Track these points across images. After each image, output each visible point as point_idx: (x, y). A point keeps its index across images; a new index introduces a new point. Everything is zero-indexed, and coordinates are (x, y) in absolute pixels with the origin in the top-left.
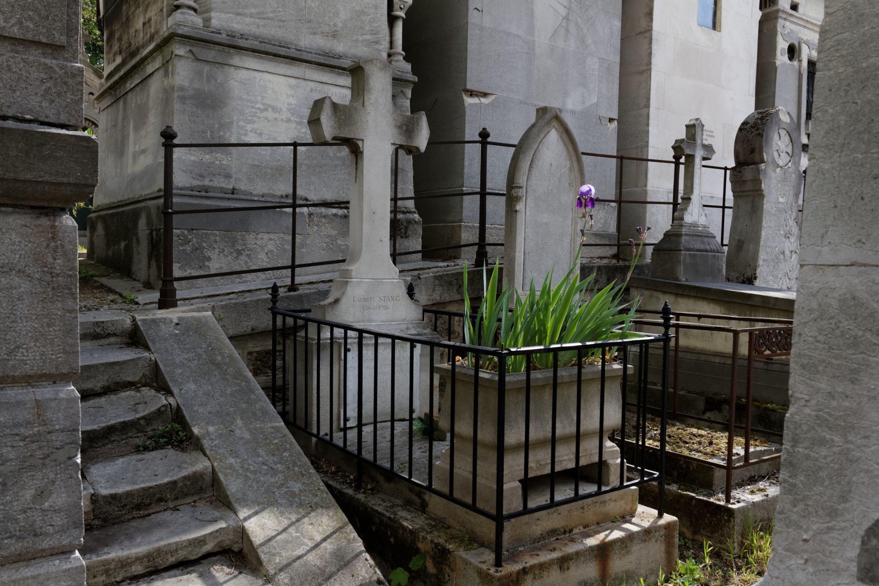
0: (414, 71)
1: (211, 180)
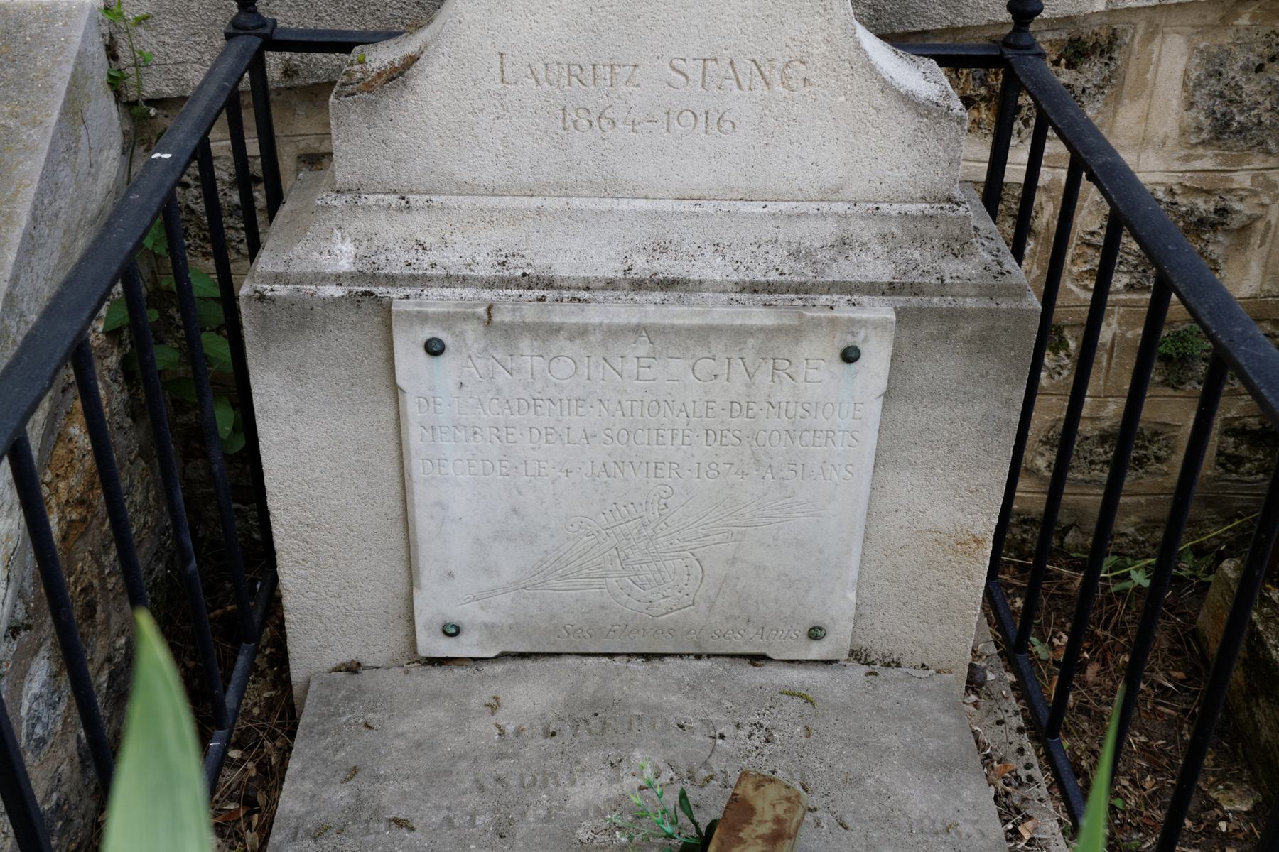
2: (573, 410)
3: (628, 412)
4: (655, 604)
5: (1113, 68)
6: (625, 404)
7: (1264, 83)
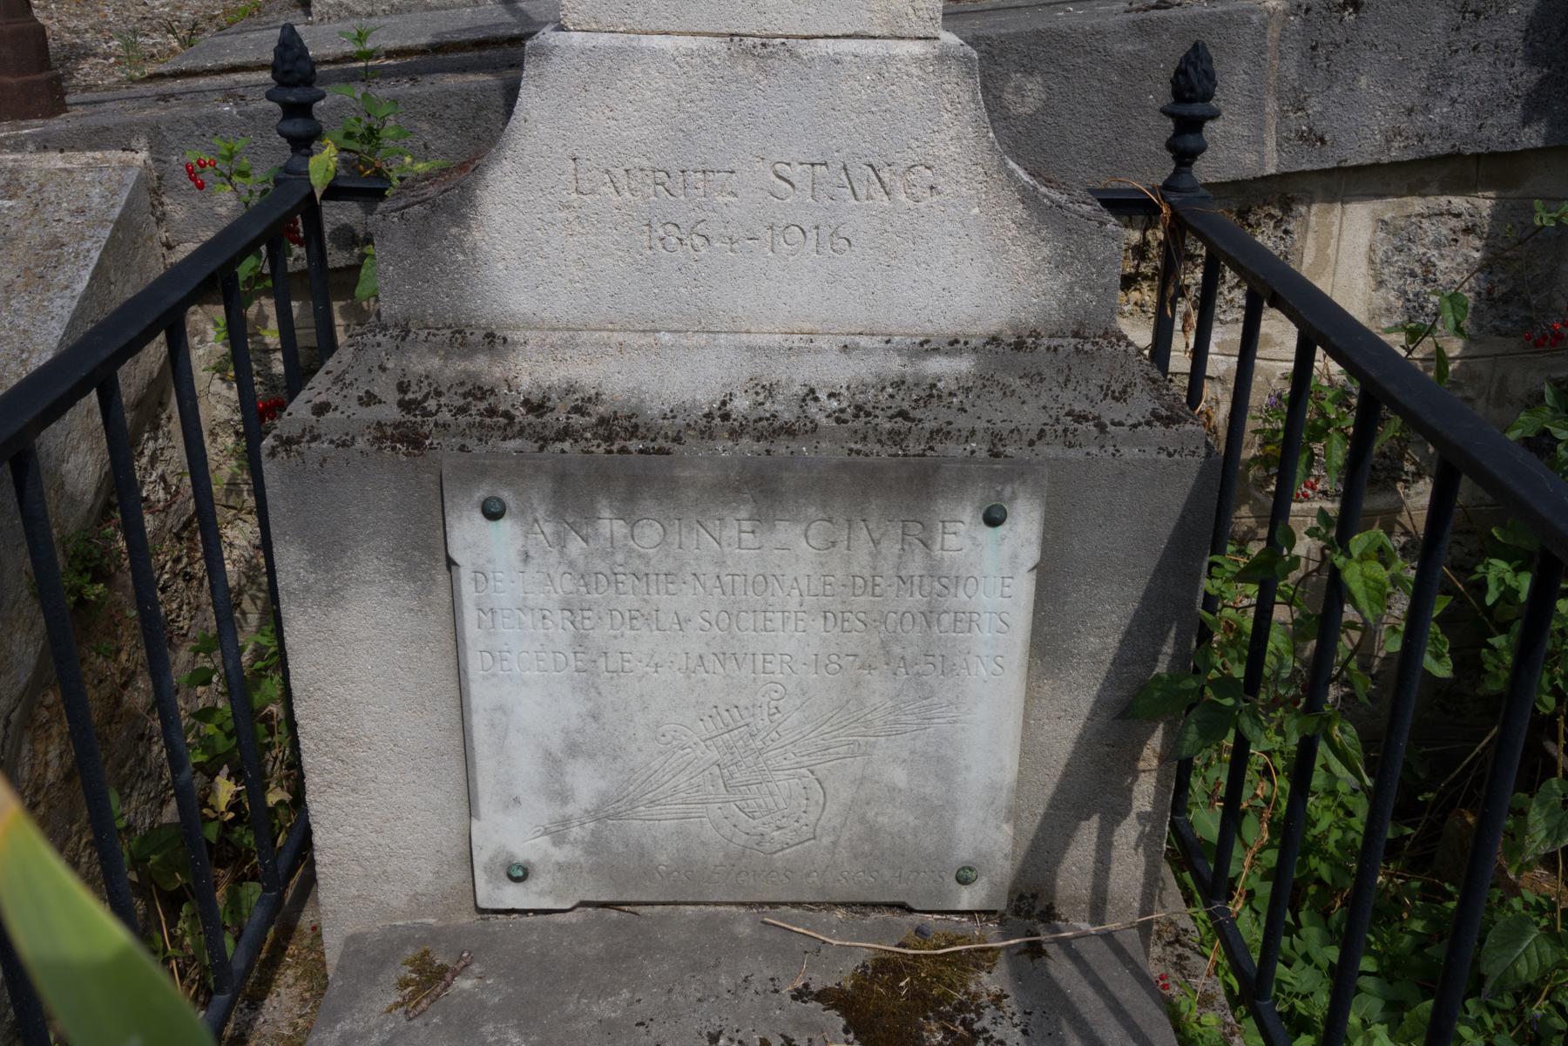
3: (729, 590)
4: (767, 838)
5: (1289, 242)
7: (1459, 259)
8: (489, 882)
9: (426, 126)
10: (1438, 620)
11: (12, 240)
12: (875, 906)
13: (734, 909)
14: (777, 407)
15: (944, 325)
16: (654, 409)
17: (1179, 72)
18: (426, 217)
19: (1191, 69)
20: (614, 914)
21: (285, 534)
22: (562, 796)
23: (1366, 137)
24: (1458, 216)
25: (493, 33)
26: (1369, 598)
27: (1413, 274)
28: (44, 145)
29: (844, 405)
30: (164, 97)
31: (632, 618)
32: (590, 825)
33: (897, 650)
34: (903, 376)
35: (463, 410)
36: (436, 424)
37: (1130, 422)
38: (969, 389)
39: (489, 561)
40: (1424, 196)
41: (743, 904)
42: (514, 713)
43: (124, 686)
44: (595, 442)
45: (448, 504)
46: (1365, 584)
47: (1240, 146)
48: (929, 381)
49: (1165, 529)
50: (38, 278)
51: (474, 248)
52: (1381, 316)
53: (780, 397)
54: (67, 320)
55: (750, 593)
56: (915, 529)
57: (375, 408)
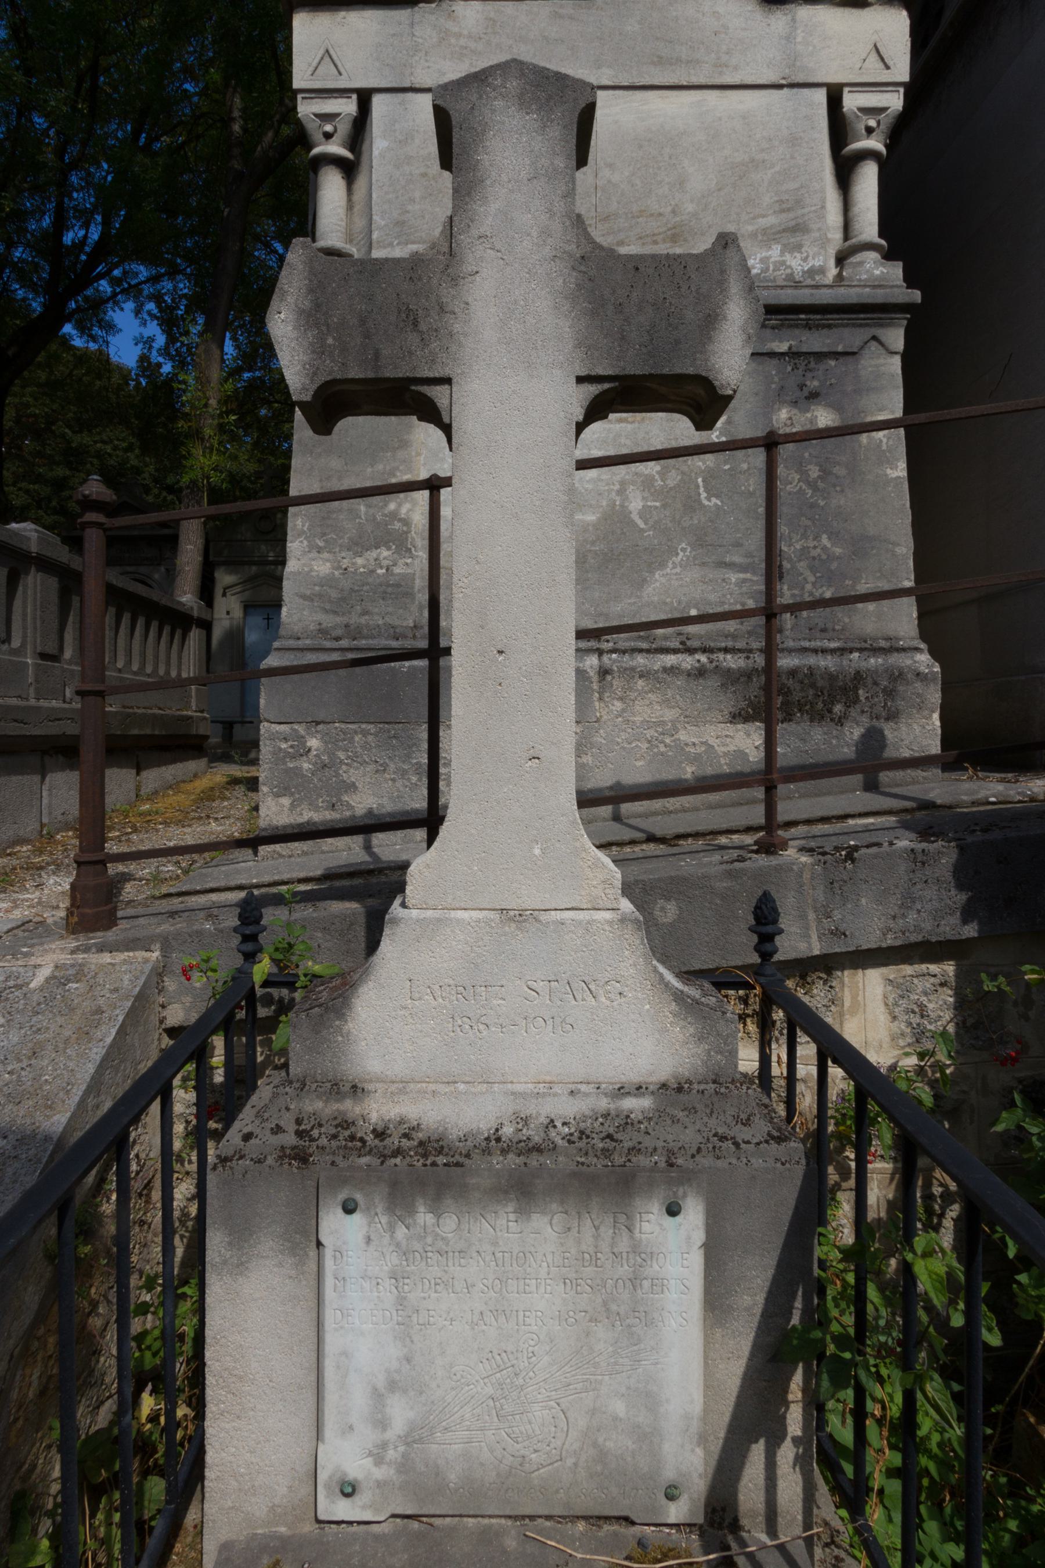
0: (911, 279)
1: (365, 613)
2: (456, 1260)
3: (500, 1263)
4: (527, 1459)
6: (499, 1255)
7: (941, 1003)
8: (327, 1497)
9: (320, 935)
10: (985, 1300)
11: (73, 1009)
12: (607, 1518)
13: (503, 1521)
14: (530, 1132)
15: (632, 1076)
16: (454, 1134)
17: (757, 908)
18: (322, 1015)
19: (764, 907)
20: (415, 1525)
21: (215, 1223)
22: (383, 1424)
23: (871, 932)
24: (935, 976)
25: (359, 868)
26: (934, 1288)
27: (913, 1012)
28: (101, 949)
29: (573, 1130)
30: (172, 914)
31: (436, 1284)
32: (401, 1449)
33: (614, 1307)
34: (609, 1110)
35: (334, 1137)
36: (318, 1147)
37: (755, 1141)
38: (650, 1119)
39: (344, 1243)
40: (911, 964)
41: (510, 1517)
42: (354, 1360)
43: (89, 1314)
44: (416, 1158)
45: (321, 1203)
46: (930, 1277)
47: (797, 940)
48: (625, 1113)
49: (786, 1215)
50: (84, 1035)
51: (349, 1032)
52: (898, 1038)
53: (532, 1126)
54: (98, 1062)
55: (515, 1265)
56: (622, 1218)
57: (281, 1136)
